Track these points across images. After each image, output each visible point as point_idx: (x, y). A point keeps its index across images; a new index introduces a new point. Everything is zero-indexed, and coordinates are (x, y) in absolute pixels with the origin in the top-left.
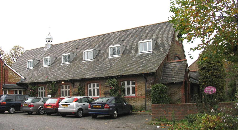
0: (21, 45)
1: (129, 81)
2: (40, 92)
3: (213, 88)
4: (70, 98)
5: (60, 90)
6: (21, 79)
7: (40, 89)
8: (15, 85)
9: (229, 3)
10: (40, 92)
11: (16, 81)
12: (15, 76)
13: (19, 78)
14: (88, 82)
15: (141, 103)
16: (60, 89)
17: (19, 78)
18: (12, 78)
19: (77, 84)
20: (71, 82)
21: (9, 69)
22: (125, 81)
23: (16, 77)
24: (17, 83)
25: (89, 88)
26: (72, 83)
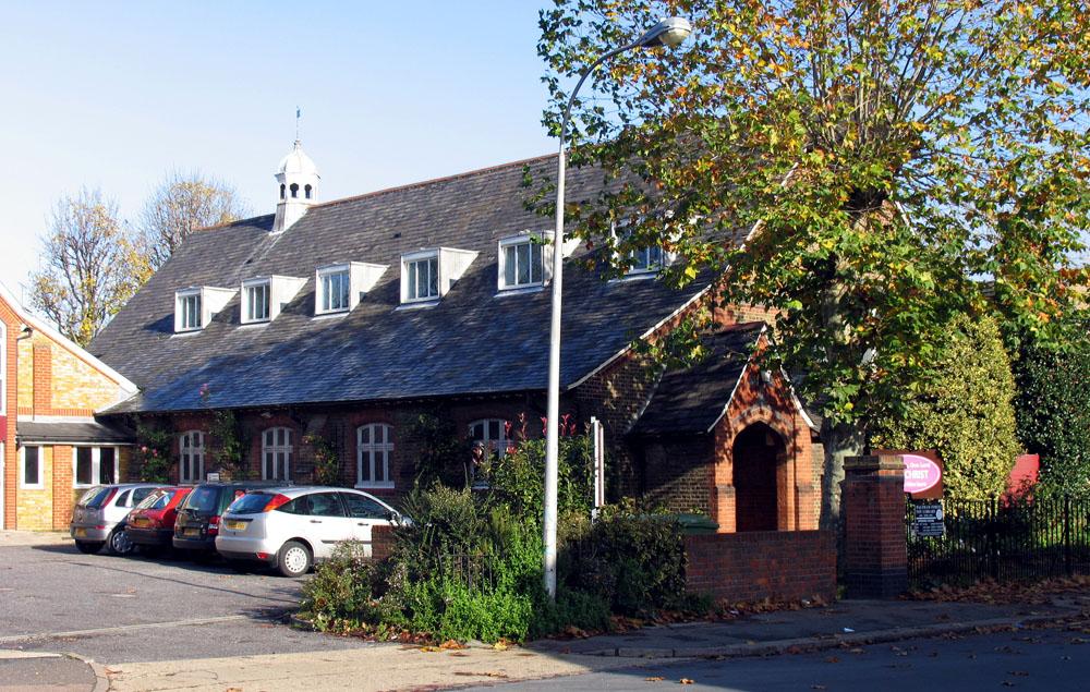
0: (208, 177)
1: (495, 420)
2: (187, 457)
3: (924, 462)
4: (797, 508)
5: (260, 453)
6: (120, 391)
7: (366, 440)
8: (92, 421)
9: (911, 64)
10: (368, 453)
11: (90, 401)
12: (87, 379)
13: (108, 387)
14: (357, 418)
15: (865, 544)
16: (260, 446)
17: (108, 387)
18: (70, 386)
19: (317, 422)
20: (296, 415)
21: (58, 347)
22: (483, 418)
23: (92, 384)
24: (98, 411)
25: (361, 447)
26: (298, 420)
